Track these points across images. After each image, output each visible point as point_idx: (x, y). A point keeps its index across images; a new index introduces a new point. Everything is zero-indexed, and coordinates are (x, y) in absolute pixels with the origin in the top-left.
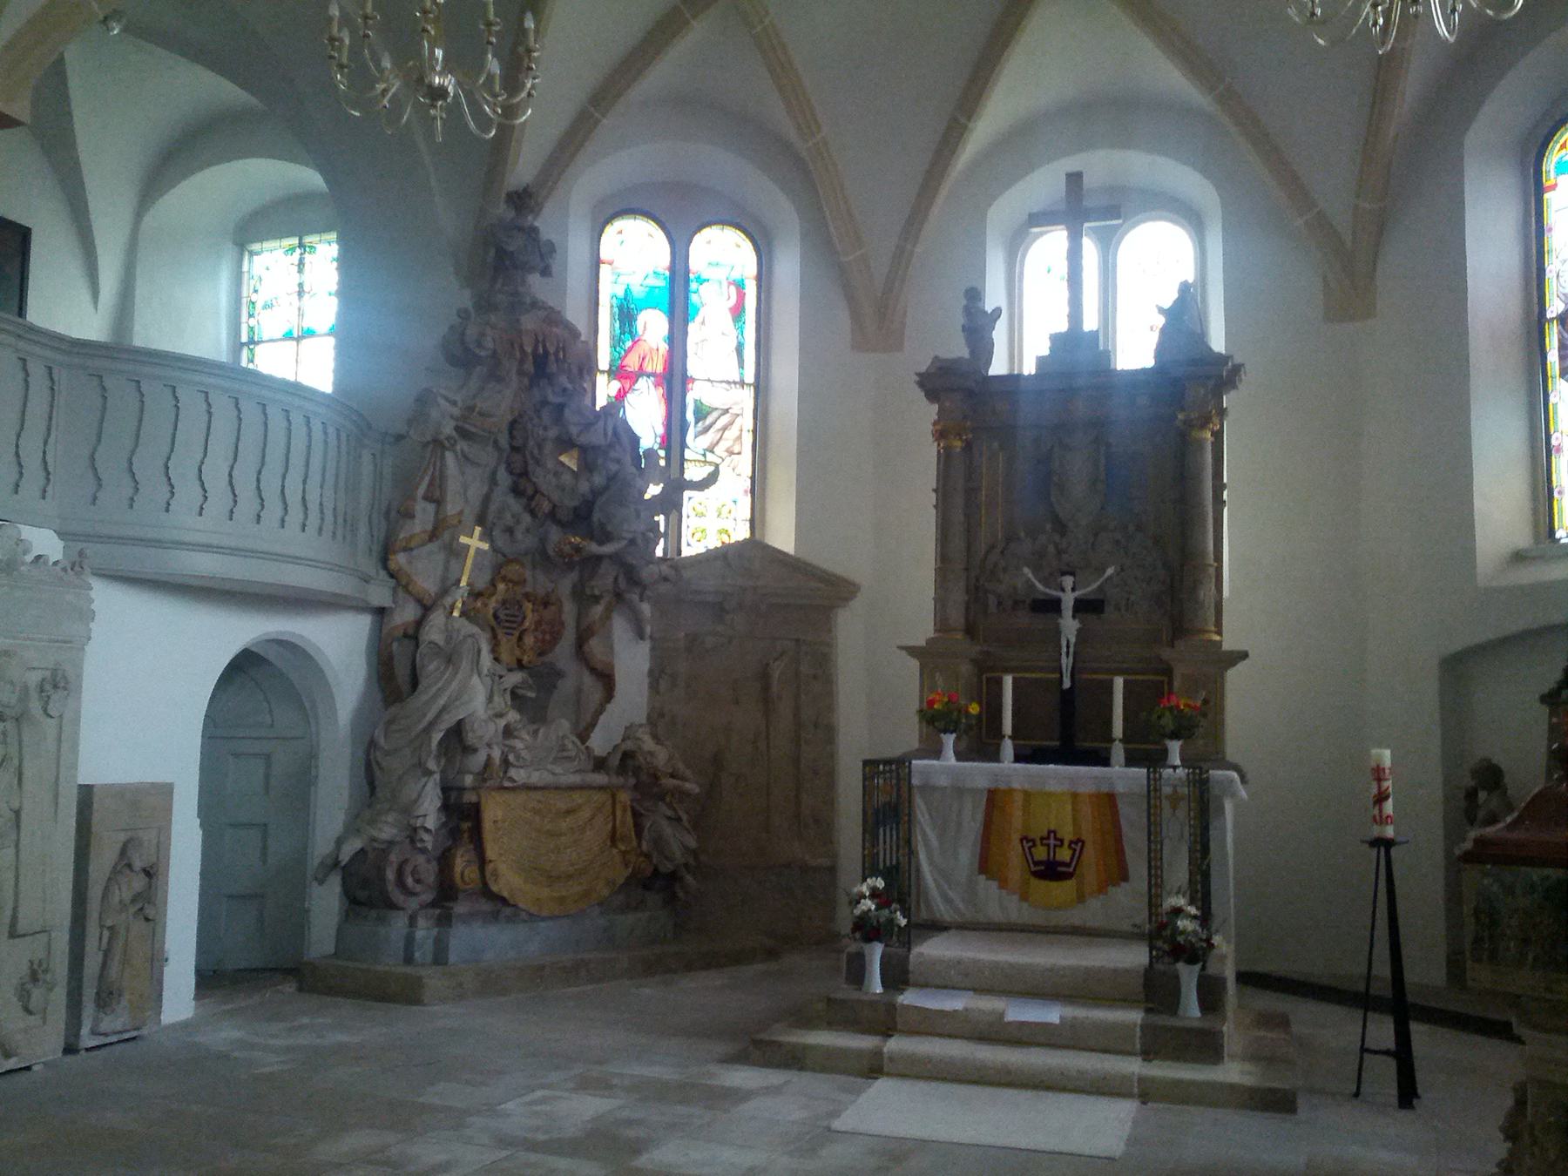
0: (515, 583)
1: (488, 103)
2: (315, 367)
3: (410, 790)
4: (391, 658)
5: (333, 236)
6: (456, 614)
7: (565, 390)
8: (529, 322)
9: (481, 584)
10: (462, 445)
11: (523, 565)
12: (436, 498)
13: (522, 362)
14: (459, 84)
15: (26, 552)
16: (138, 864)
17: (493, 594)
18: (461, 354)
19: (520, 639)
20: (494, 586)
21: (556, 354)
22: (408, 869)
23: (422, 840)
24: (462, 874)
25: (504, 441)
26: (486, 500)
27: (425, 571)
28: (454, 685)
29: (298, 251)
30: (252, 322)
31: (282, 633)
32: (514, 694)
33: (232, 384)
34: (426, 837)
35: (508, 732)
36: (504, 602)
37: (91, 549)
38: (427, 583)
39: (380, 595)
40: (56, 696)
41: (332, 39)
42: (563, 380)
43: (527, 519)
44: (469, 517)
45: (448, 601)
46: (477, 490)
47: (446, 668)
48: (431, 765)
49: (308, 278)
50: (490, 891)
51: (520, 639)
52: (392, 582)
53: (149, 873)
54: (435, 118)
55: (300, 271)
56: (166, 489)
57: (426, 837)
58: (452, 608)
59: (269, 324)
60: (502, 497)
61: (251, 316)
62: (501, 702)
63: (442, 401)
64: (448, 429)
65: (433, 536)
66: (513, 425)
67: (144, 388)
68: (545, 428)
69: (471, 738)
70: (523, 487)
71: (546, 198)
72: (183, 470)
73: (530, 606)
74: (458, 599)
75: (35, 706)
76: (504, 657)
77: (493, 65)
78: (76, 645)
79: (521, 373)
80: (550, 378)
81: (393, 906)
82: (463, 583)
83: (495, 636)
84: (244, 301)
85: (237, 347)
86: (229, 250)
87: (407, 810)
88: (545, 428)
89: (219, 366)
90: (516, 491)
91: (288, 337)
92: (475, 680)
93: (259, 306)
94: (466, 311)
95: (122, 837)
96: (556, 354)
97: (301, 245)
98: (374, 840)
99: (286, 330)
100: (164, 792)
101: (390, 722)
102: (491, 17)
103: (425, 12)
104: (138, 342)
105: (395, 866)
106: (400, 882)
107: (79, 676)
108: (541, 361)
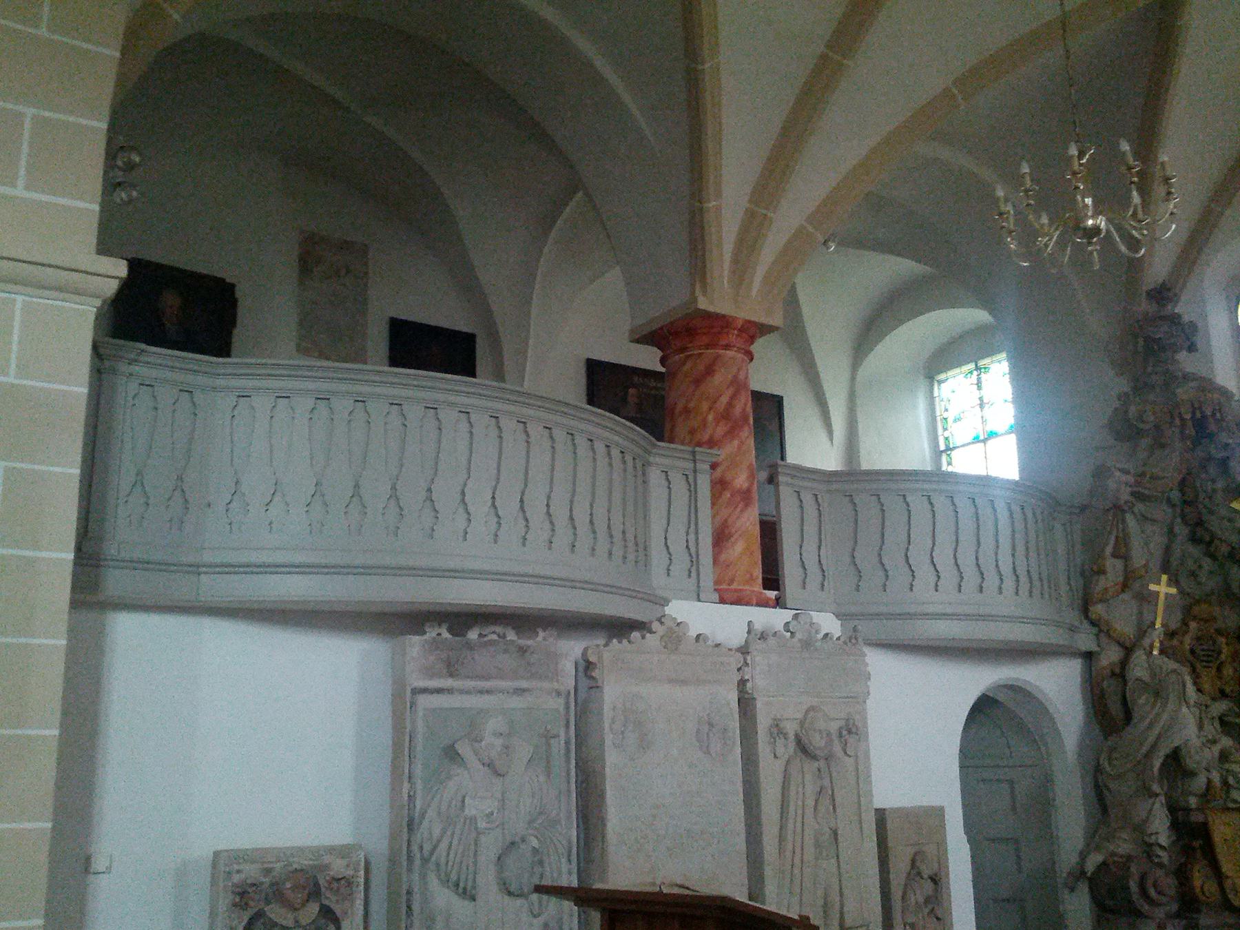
0: (1206, 621)
1: (1135, 228)
2: (1002, 461)
3: (1141, 809)
4: (1102, 695)
5: (1004, 355)
6: (1155, 653)
7: (1227, 445)
8: (1184, 393)
9: (1174, 625)
10: (1140, 507)
11: (1210, 604)
12: (1122, 553)
13: (1183, 426)
14: (1109, 220)
15: (817, 632)
16: (926, 873)
17: (1186, 632)
18: (1126, 429)
19: (1219, 669)
20: (1186, 625)
21: (1214, 415)
22: (1150, 882)
23: (1159, 856)
24: (1202, 888)
25: (1175, 495)
26: (1168, 550)
27: (1122, 617)
28: (1165, 716)
29: (975, 373)
30: (947, 434)
31: (1017, 679)
32: (1222, 722)
33: (935, 482)
34: (1161, 853)
35: (1224, 757)
36: (1198, 639)
37: (865, 628)
38: (1124, 625)
39: (1086, 641)
40: (851, 740)
41: (1001, 214)
42: (1224, 437)
43: (1207, 563)
44: (1155, 565)
45: (1146, 642)
46: (1158, 541)
47: (1156, 701)
48: (1156, 788)
49: (986, 392)
50: (1231, 904)
51: (1219, 669)
52: (1095, 630)
53: (935, 880)
54: (1091, 253)
55: (979, 388)
56: (881, 573)
57: (1161, 853)
58: (1152, 647)
59: (959, 433)
60: (1181, 545)
61: (945, 429)
62: (1211, 729)
63: (1118, 474)
64: (1125, 496)
65: (1125, 586)
66: (1183, 484)
67: (908, 499)
68: (1213, 481)
69: (1190, 764)
70: (1201, 535)
71: (1181, 290)
72: (919, 557)
73: (1224, 640)
74: (1156, 638)
75: (837, 748)
76: (1206, 687)
77: (1136, 198)
78: (859, 699)
79: (1183, 437)
80: (1210, 436)
81: (1139, 914)
82: (1158, 625)
83: (1194, 670)
84: (938, 419)
85: (937, 454)
86: (922, 384)
87: (1140, 828)
88: (1213, 481)
89: (924, 473)
90: (1194, 539)
91: (976, 440)
92: (1184, 709)
93: (950, 421)
94: (1126, 394)
95: (910, 851)
96: (1214, 415)
97: (977, 368)
98: (1113, 854)
99: (974, 434)
100: (937, 814)
101: (1112, 750)
102: (1131, 161)
103: (1074, 173)
104: (865, 466)
105: (1136, 878)
106: (1144, 892)
107: (864, 719)
108: (1200, 424)
